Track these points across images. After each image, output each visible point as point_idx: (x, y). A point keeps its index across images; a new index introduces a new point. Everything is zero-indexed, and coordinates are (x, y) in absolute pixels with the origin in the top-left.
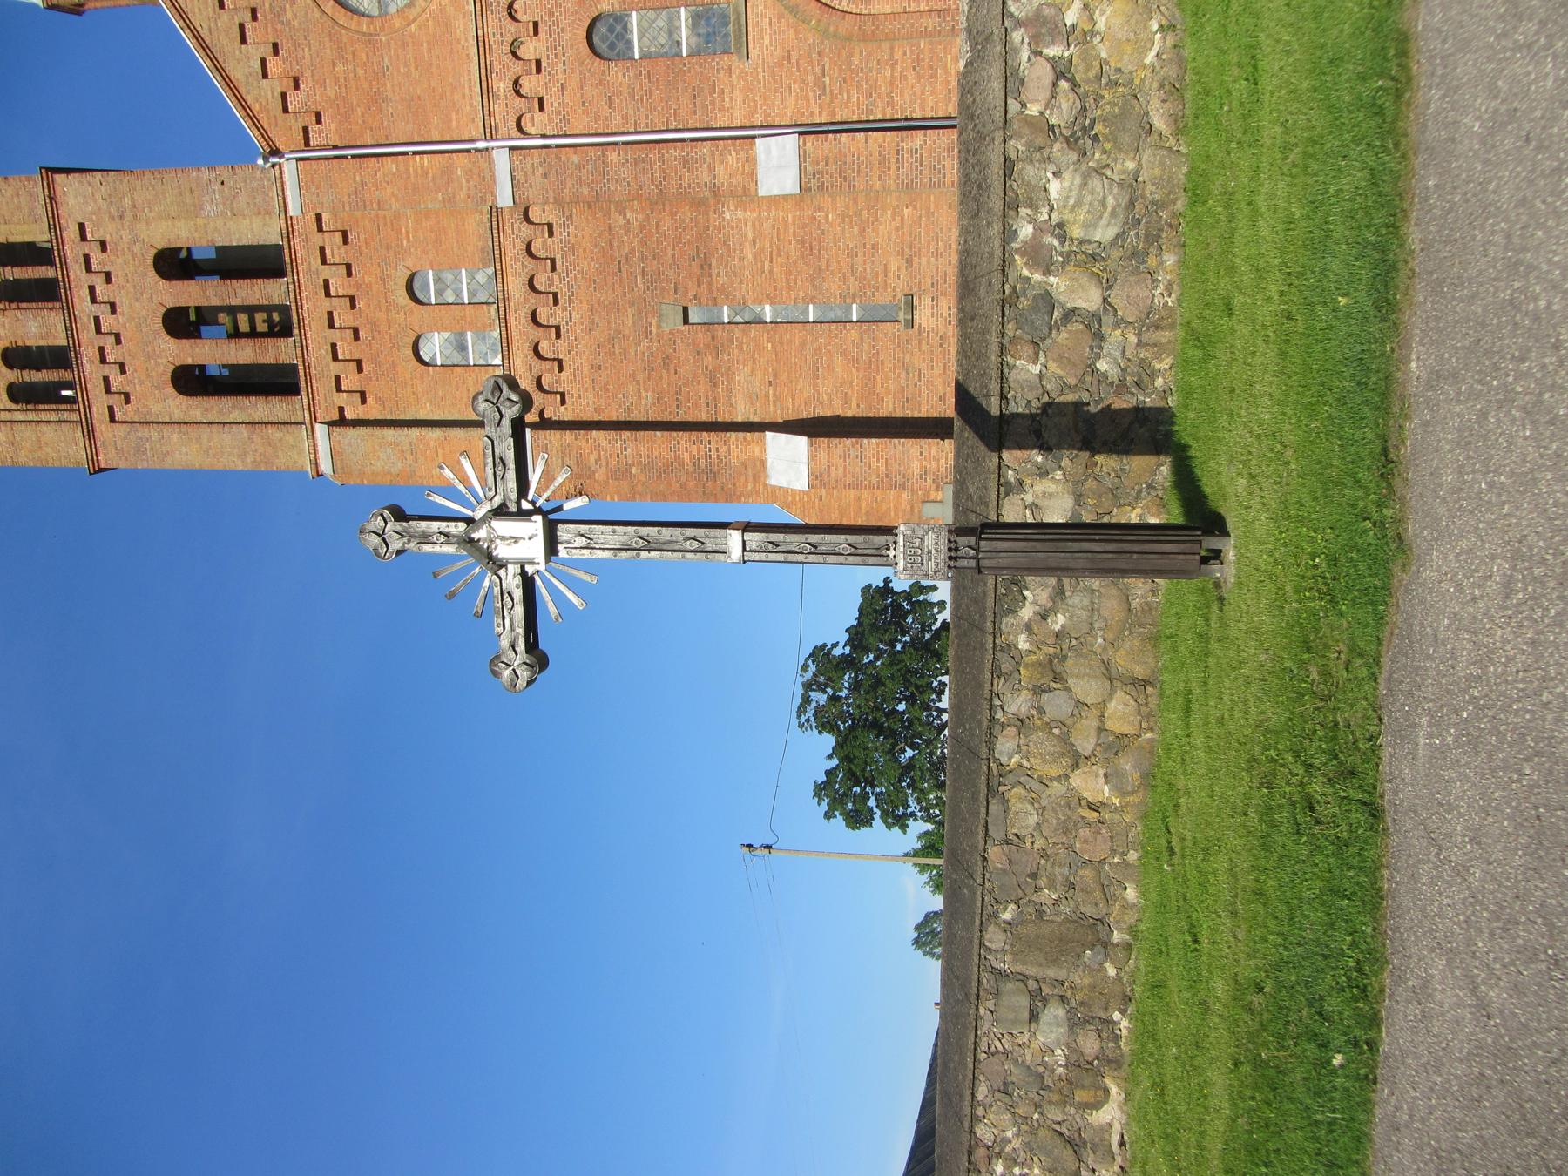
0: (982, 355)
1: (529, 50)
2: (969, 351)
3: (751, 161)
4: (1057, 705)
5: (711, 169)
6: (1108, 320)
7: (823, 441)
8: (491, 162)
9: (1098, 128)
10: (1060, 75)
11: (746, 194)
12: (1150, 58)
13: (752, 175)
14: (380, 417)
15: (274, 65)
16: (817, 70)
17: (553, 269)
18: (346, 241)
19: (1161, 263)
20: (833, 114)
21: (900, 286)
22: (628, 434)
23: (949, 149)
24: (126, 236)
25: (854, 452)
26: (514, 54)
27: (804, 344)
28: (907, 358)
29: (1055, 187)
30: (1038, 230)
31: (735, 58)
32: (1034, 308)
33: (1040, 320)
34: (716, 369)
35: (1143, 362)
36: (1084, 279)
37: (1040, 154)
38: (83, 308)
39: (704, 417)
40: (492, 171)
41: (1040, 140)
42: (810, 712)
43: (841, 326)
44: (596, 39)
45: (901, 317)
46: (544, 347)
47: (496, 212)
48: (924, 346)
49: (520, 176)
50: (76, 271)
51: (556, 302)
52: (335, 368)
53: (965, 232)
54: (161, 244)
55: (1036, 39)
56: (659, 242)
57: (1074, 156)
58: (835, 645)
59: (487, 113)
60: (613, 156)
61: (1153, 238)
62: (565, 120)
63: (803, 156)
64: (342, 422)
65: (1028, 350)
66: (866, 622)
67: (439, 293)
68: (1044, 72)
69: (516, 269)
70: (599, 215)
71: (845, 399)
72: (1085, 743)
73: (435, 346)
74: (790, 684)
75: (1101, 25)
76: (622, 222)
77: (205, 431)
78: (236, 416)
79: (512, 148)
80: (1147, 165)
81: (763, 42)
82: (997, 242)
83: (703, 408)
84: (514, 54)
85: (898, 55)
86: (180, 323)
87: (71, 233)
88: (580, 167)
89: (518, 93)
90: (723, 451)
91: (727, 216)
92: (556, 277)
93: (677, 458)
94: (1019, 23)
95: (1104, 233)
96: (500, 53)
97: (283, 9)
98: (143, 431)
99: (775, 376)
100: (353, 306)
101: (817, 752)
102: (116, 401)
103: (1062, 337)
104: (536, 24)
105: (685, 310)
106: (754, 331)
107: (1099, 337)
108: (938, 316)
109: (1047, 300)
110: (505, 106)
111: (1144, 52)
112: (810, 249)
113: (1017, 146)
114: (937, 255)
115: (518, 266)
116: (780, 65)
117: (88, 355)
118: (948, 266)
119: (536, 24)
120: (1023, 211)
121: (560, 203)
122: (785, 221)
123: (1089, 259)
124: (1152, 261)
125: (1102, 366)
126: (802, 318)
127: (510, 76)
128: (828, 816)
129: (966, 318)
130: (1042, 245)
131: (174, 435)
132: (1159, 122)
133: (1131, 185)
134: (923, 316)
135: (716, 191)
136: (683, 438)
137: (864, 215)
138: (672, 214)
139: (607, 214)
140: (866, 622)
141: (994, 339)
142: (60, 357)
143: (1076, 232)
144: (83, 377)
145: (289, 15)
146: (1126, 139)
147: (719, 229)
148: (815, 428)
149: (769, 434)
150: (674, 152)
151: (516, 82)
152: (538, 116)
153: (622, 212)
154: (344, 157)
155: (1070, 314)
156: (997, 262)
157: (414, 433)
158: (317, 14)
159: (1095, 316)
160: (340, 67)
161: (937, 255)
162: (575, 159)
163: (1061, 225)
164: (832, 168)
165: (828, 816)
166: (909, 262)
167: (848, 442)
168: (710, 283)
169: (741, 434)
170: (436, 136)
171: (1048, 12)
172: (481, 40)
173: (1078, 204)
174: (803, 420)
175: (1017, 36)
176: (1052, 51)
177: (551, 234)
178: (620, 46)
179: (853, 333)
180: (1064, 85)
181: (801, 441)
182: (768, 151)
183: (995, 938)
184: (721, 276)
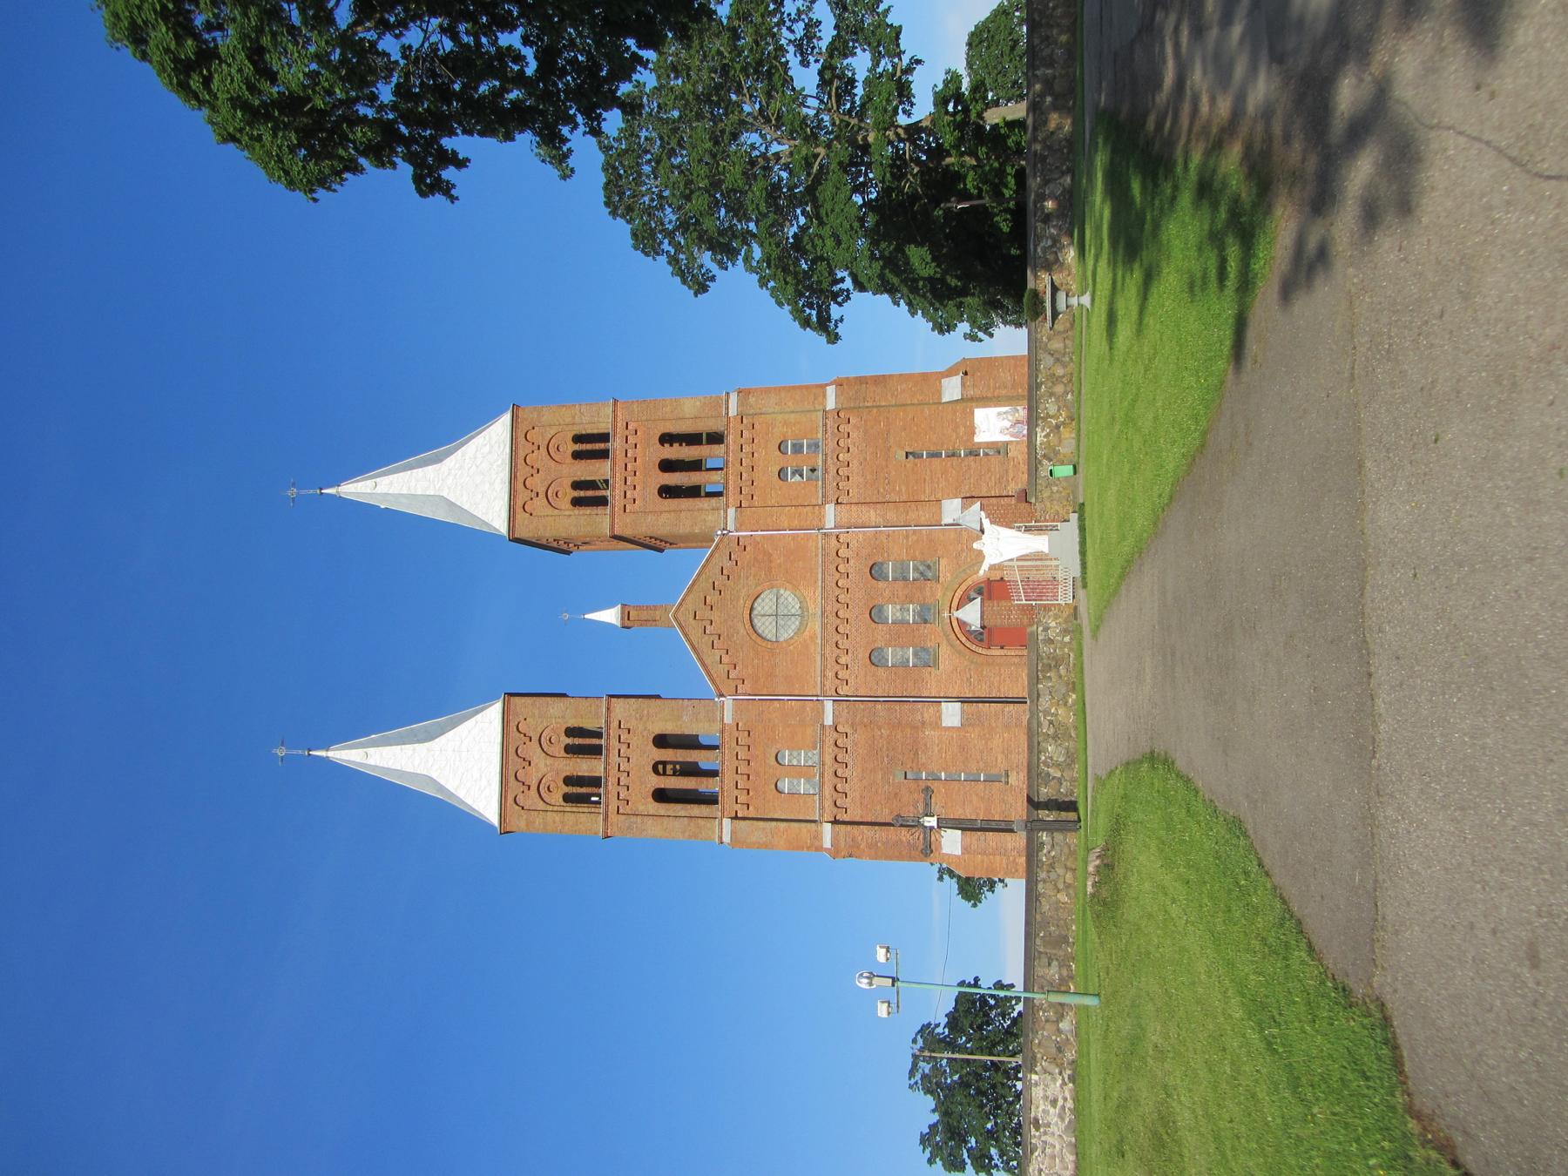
1: (843, 660)
2: (1030, 786)
3: (939, 711)
4: (1053, 876)
11: (937, 723)
15: (725, 659)
21: (1002, 765)
24: (641, 727)
37: (1046, 740)
38: (614, 758)
42: (918, 1076)
46: (839, 787)
47: (823, 726)
50: (614, 742)
52: (736, 792)
54: (658, 731)
58: (937, 1025)
59: (823, 685)
60: (879, 706)
63: (963, 712)
64: (736, 818)
66: (961, 1009)
69: (830, 750)
72: (1061, 886)
73: (785, 785)
74: (904, 1049)
77: (666, 820)
78: (682, 813)
86: (658, 768)
87: (615, 724)
96: (831, 661)
98: (633, 819)
101: (923, 1111)
102: (622, 804)
109: (1048, 774)
112: (962, 748)
117: (612, 780)
121: (852, 725)
123: (1058, 765)
128: (931, 1161)
129: (1029, 778)
131: (650, 821)
133: (1067, 749)
135: (923, 723)
140: (961, 1009)
142: (595, 782)
144: (607, 793)
150: (906, 706)
165: (931, 1161)
179: (982, 786)
183: (1038, 941)
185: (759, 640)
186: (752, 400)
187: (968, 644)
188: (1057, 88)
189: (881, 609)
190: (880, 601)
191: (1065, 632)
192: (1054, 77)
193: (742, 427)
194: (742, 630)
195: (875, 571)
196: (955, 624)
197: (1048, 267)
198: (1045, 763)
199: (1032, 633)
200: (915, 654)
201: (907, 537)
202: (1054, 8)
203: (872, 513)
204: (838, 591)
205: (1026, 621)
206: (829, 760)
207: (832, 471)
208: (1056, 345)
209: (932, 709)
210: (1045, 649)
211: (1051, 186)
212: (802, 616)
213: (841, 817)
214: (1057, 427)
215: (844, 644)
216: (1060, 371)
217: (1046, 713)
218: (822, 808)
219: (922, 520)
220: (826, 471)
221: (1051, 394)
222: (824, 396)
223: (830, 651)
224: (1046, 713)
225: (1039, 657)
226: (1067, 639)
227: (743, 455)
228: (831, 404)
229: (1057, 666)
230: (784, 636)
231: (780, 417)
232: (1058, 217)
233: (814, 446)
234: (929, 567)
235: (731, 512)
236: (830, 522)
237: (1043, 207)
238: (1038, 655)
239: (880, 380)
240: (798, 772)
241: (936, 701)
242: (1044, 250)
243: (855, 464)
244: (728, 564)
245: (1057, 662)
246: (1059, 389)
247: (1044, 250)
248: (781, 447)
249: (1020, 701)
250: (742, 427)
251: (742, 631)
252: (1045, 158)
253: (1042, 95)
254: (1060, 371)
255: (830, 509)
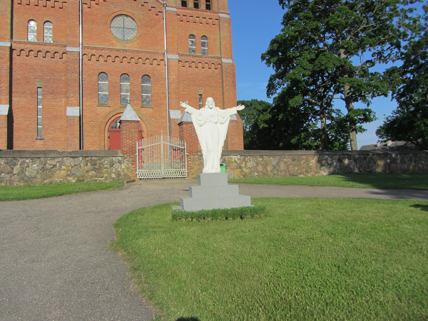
0: (5, 154)
3: (75, 105)
5: (73, 97)
6: (11, 175)
7: (6, 119)
8: (77, 47)
9: (45, 172)
10: (54, 166)
11: (68, 104)
12: (56, 179)
13: (71, 106)
14: (14, 7)
16: (94, 121)
17: (52, 58)
18: (60, 8)
19: (22, 183)
20: (85, 123)
22: (9, 71)
23: (75, 148)
25: (3, 126)
26: (100, 56)
27: (32, 115)
28: (28, 139)
29: (35, 165)
30: (28, 163)
31: (97, 103)
32: (14, 163)
33: (12, 163)
34: (26, 94)
35: (3, 181)
36: (19, 171)
37: (41, 163)
39: (13, 90)
40: (75, 47)
41: (43, 163)
43: (36, 123)
44: (103, 74)
45: (38, 137)
47: (65, 46)
48: (31, 142)
49: (73, 53)
51: (43, 57)
53: (30, 151)
55: (60, 162)
56: (57, 83)
57: (40, 168)
59: (88, 48)
60: (77, 75)
61: (26, 181)
62: (86, 65)
63: (75, 117)
65: (6, 162)
67: (47, 28)
68: (54, 163)
69: (53, 49)
70: (64, 70)
71: (18, 124)
75: (62, 172)
76: (62, 75)
79: (79, 52)
80: (39, 179)
81: (100, 110)
82: (25, 156)
83: (16, 90)
84: (100, 56)
85: (96, 137)
88: (75, 67)
89: (92, 55)
90: (4, 94)
91: (63, 99)
92: (50, 58)
93: (2, 83)
94: (62, 159)
95: (27, 174)
97: (113, 5)
99: (24, 108)
100: (44, 6)
103: (8, 167)
104: (106, 61)
105: (41, 88)
106: (36, 103)
107: (8, 173)
108: (39, 145)
109: (15, 165)
110: (89, 52)
111: (57, 178)
113: (42, 159)
114: (53, 145)
115: (53, 49)
116: (96, 113)
118: (51, 148)
119: (106, 61)
120: (31, 161)
121: (67, 61)
122: (61, 112)
123: (22, 171)
124: (22, 181)
125: (3, 174)
126: (39, 115)
127: (95, 54)
130: (25, 164)
132: (45, 181)
133: (35, 177)
134: (39, 142)
135: (68, 97)
136: (8, 84)
137: (62, 130)
138: (64, 87)
139: (64, 72)
141: (8, 156)
143: (27, 169)
145: (112, 6)
146: (43, 176)
147: (60, 97)
148: (10, 117)
149: (8, 106)
150: (77, 89)
151: (94, 55)
152: (87, 59)
153: (65, 75)
154: (80, 12)
155: (13, 169)
156: (22, 156)
157: (10, 16)
158: (112, 12)
159: (12, 173)
160: (100, 15)
161: (53, 145)
162: (77, 67)
163: (28, 167)
164: (72, 123)
166: (52, 139)
167: (6, 125)
168: (47, 94)
169: (8, 99)
170: (84, 35)
171: (64, 164)
172: (103, 49)
173: (32, 169)
174: (12, 114)
175: (60, 159)
176: (58, 164)
177: (60, 58)
178: (101, 79)
179: (35, 126)
180: (52, 166)
181: (6, 113)
182: (76, 109)
184: (50, 97)
185: (111, 18)
186: (226, 25)
187: (109, 124)
188: (393, 165)
189: (127, 80)
190: (131, 79)
191: (118, 174)
192: (397, 164)
193: (214, 19)
194: (117, 10)
195: (146, 77)
196: (118, 115)
197: (319, 161)
198: (24, 162)
199: (117, 153)
200: (105, 95)
201: (162, 93)
202: (422, 163)
203: (175, 77)
204: (136, 58)
205: (125, 149)
206: (47, 48)
207: (194, 59)
208: (282, 166)
209: (76, 102)
210: (106, 162)
211: (354, 163)
212: (124, 40)
213: (15, 54)
214: (240, 167)
215: (110, 60)
216: (269, 168)
217: (62, 163)
218: (20, 43)
219: (171, 101)
220: (194, 56)
221: (257, 164)
222: (228, 58)
223: (105, 53)
224: (62, 163)
225: (101, 158)
226: (113, 176)
227: (201, 18)
228: (224, 60)
229: (94, 169)
230: (113, 31)
231: (218, 37)
232: (340, 166)
233: (204, 52)
234: (149, 103)
235: (175, 10)
236: (171, 56)
237: (345, 158)
238: (102, 157)
239: (234, 83)
240: (40, 33)
241: (80, 104)
242: (326, 160)
243: (197, 70)
244: (149, 6)
245: (98, 170)
246: (260, 168)
247: (326, 160)
248: (204, 37)
249: (81, 147)
250: (214, 19)
251: (116, 10)
252: (366, 160)
253: (391, 158)
254: (269, 168)
255: (176, 57)
